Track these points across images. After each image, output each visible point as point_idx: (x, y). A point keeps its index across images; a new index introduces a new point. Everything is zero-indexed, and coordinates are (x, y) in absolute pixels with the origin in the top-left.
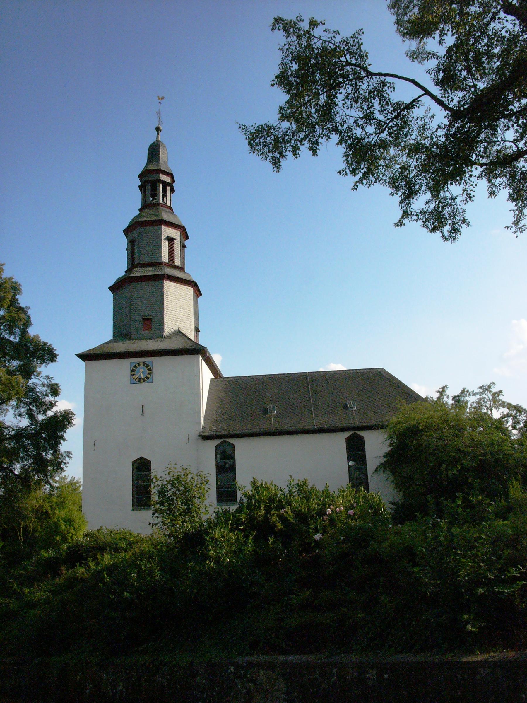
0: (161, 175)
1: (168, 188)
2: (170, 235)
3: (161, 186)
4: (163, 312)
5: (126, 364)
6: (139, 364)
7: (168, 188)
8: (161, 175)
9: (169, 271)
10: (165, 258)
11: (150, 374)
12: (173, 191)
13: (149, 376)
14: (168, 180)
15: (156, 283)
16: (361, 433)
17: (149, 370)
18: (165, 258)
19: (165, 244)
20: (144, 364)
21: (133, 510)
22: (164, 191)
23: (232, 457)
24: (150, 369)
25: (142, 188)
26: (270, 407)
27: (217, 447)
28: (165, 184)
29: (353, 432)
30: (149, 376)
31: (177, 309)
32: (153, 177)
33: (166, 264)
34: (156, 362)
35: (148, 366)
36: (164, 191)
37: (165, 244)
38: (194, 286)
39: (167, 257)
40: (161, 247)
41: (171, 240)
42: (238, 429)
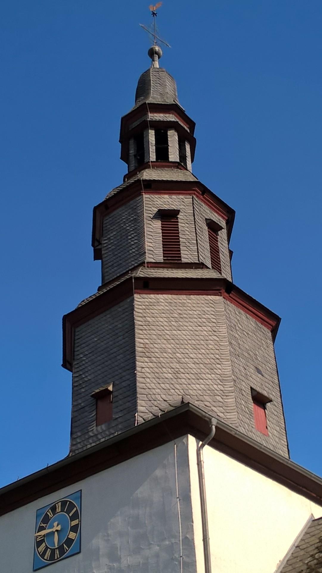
1: (173, 137)
4: (134, 368)
6: (54, 509)
7: (173, 137)
11: (75, 529)
12: (186, 139)
13: (72, 535)
17: (72, 518)
20: (64, 503)
24: (76, 516)
28: (161, 130)
30: (72, 535)
33: (156, 265)
40: (140, 235)
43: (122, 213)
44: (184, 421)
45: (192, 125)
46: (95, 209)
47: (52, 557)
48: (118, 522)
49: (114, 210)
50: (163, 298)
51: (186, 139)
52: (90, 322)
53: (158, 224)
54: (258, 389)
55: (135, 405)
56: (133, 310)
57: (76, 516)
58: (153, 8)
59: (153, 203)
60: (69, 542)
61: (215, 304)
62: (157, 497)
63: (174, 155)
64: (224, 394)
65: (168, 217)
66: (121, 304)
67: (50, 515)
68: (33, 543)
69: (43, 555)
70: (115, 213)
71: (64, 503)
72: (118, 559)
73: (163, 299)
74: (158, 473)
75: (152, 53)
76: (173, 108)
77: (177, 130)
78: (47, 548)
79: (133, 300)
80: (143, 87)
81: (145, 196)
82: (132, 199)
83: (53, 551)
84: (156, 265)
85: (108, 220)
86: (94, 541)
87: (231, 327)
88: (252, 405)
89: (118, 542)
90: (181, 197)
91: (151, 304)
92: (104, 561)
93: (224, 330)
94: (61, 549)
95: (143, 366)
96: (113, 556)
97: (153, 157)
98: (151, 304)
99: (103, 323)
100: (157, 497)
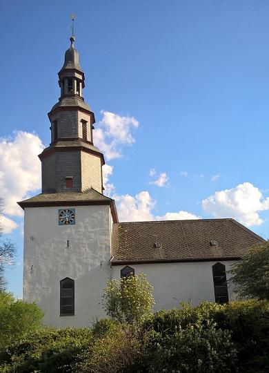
3: (67, 80)
5: (55, 211)
6: (65, 211)
10: (80, 135)
11: (73, 218)
14: (80, 77)
15: (75, 153)
16: (223, 263)
18: (80, 135)
19: (80, 125)
20: (69, 211)
37: (80, 125)
76: (82, 74)
96: (86, 227)
100: (99, 217)
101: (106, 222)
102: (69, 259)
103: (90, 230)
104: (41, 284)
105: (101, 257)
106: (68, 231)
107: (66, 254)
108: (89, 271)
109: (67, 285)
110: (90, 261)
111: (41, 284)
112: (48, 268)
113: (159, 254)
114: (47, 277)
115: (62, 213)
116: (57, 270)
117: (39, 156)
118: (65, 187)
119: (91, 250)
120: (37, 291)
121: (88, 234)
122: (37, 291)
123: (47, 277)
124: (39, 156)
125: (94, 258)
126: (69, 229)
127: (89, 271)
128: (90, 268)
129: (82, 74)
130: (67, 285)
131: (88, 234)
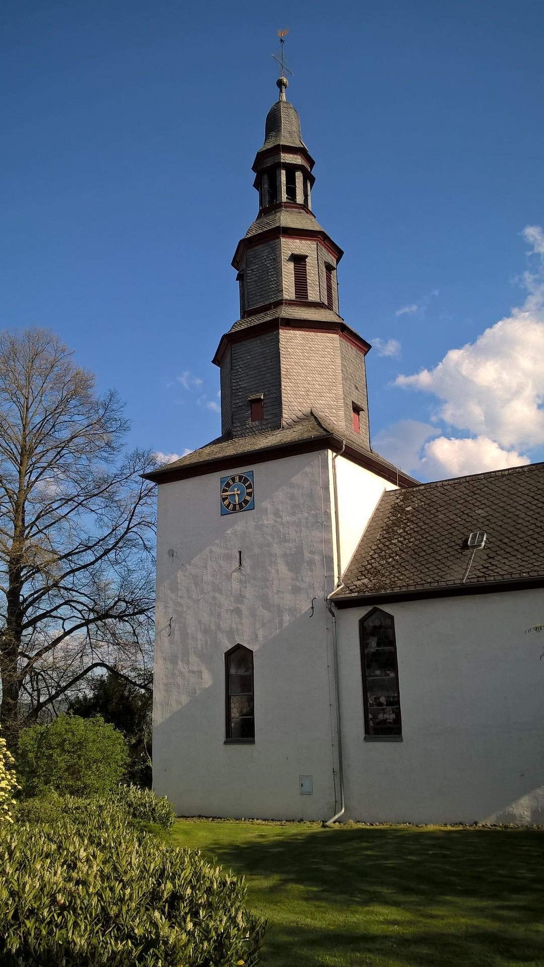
0: (282, 155)
1: (299, 176)
2: (297, 252)
3: (283, 172)
4: (280, 385)
5: (213, 481)
6: (233, 479)
7: (299, 176)
8: (282, 155)
9: (287, 312)
10: (289, 290)
11: (250, 494)
12: (309, 178)
13: (248, 498)
14: (297, 160)
15: (267, 338)
16: (387, 609)
17: (248, 487)
18: (289, 290)
19: (288, 270)
20: (240, 478)
21: (225, 743)
22: (291, 180)
23: (390, 641)
24: (250, 487)
25: (258, 184)
26: (474, 538)
27: (362, 622)
28: (291, 170)
29: (370, 608)
30: (248, 498)
31: (311, 374)
32: (269, 162)
33: (290, 303)
34: (260, 472)
35: (246, 480)
36: (291, 180)
37: (288, 270)
38: (342, 331)
39: (293, 290)
40: (279, 274)
41: (299, 260)
42: (406, 581)
43: (262, 250)
44: (323, 441)
45: (312, 163)
46: (241, 241)
47: (234, 509)
48: (280, 495)
49: (257, 245)
50: (298, 333)
51: (309, 178)
52: (244, 343)
53: (291, 265)
54: (356, 402)
55: (281, 412)
56: (279, 341)
57: (250, 487)
58: (281, 34)
59: (289, 246)
60: (246, 502)
61: (333, 340)
62: (306, 484)
63: (300, 199)
64: (338, 409)
65: (299, 260)
66: (268, 335)
67: (231, 483)
68: (219, 499)
69: (228, 506)
70: (256, 248)
71: (240, 478)
72: (281, 517)
73: (298, 333)
74: (307, 469)
75: (280, 84)
76: (301, 151)
77: (302, 172)
78: (230, 503)
79: (278, 334)
80: (273, 123)
81: (283, 240)
82: (272, 240)
83: (235, 506)
84: (290, 303)
85: (250, 253)
86: (262, 502)
87: (343, 358)
88: (352, 414)
89: (280, 507)
90: (309, 242)
91: (291, 338)
92: (271, 516)
93: (339, 361)
94: (240, 504)
95: (286, 386)
96: (277, 514)
97: (284, 197)
98: (291, 338)
99: (255, 346)
100: (306, 484)
101: (321, 492)
102: (240, 598)
103: (286, 518)
104: (188, 663)
105: (312, 586)
106: (239, 527)
107: (236, 586)
108: (286, 624)
109: (239, 659)
110: (288, 600)
111: (188, 663)
112: (200, 622)
113: (464, 572)
114: (199, 646)
115: (228, 485)
116: (218, 626)
117: (214, 362)
118: (249, 422)
119: (290, 570)
120: (179, 680)
121: (280, 527)
122: (179, 680)
123: (199, 646)
124: (214, 362)
125: (296, 590)
126: (243, 522)
127: (286, 624)
128: (287, 618)
129: (301, 151)
130: (239, 659)
131: (280, 527)
